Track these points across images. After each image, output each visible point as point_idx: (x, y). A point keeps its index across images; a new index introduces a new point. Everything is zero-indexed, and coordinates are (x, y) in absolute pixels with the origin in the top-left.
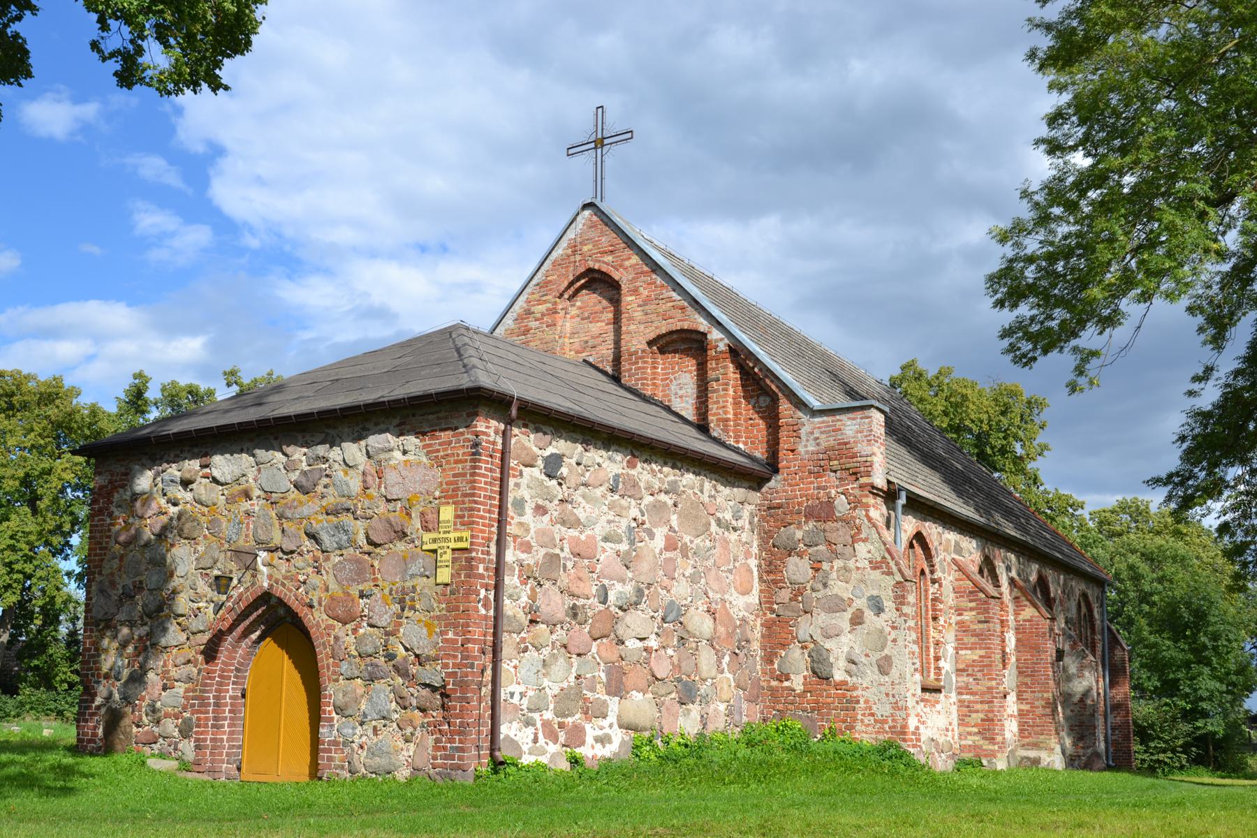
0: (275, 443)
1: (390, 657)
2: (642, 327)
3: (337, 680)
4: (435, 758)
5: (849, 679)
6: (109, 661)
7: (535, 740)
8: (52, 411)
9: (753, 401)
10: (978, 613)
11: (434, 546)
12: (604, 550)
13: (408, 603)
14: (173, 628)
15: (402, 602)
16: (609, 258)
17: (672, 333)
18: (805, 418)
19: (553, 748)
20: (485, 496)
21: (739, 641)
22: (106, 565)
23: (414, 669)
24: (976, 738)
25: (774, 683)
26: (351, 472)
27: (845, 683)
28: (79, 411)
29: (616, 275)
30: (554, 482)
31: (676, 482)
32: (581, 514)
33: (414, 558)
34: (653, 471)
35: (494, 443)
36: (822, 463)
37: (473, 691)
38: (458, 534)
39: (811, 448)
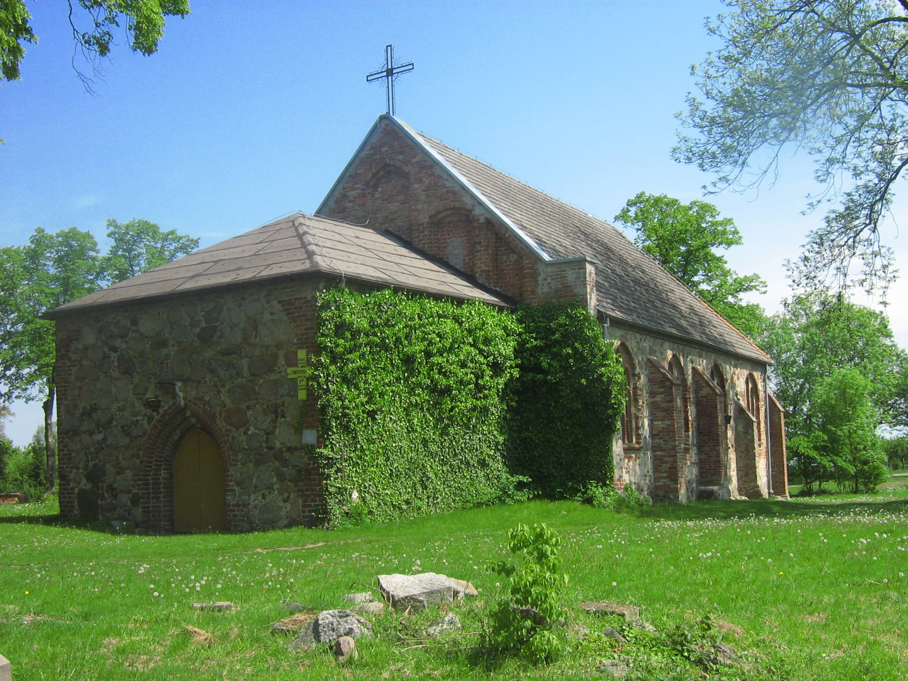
2: (426, 206)
3: (236, 465)
4: (304, 512)
10: (666, 396)
11: (295, 376)
15: (276, 412)
16: (401, 157)
24: (666, 480)
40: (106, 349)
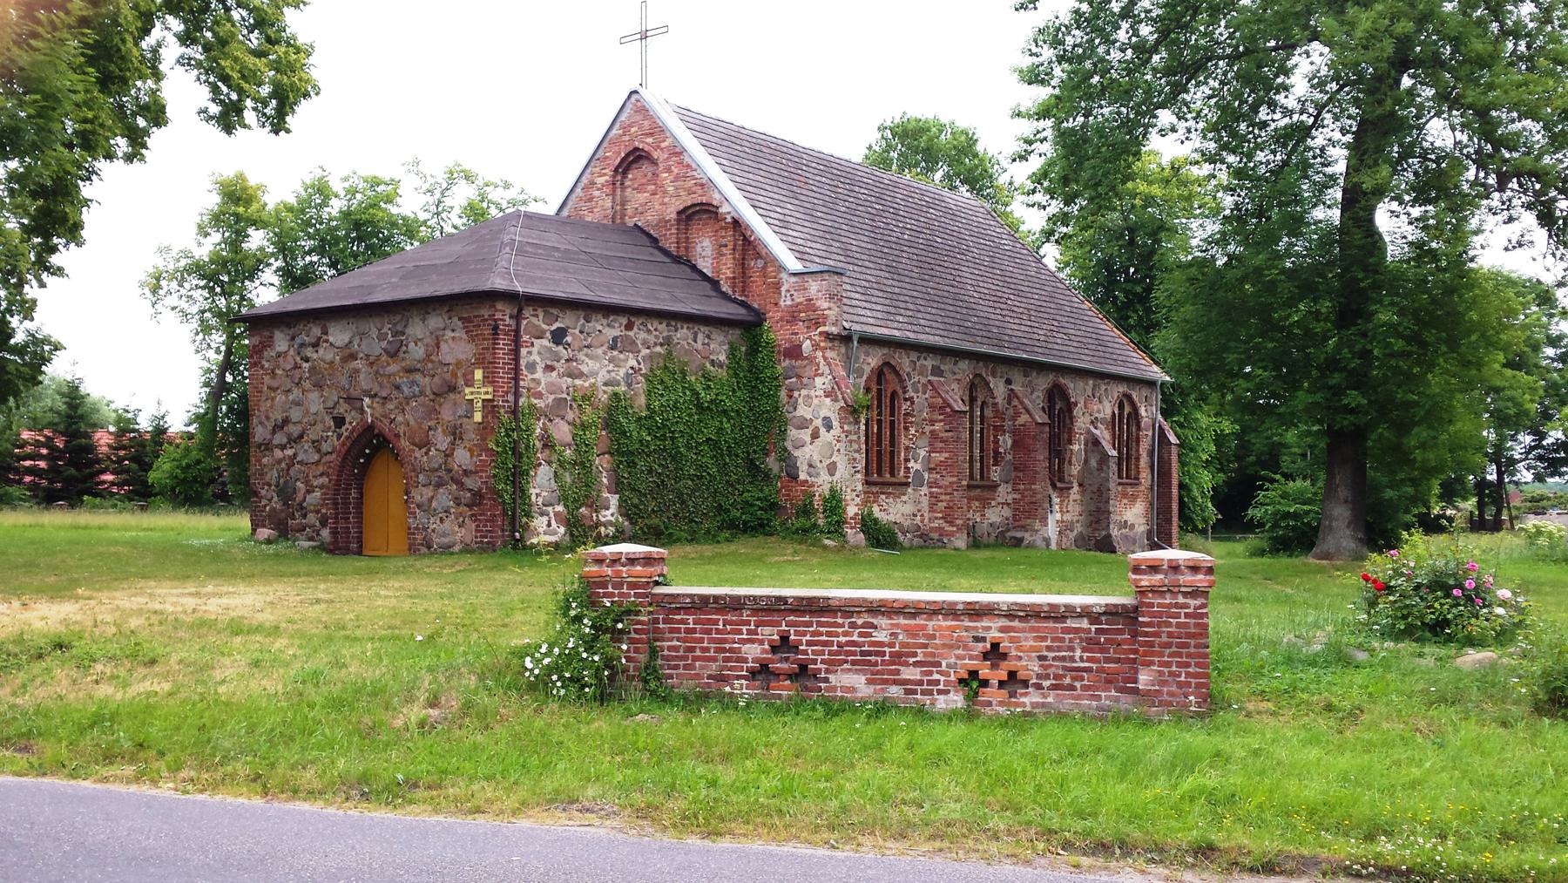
7: (549, 525)
15: (454, 434)
16: (650, 140)
17: (694, 205)
29: (655, 155)
30: (561, 348)
32: (584, 369)
40: (298, 359)
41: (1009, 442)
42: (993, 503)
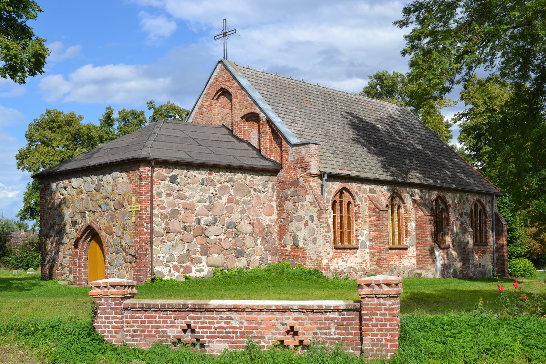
0: (88, 174)
1: (122, 246)
3: (108, 254)
4: (134, 278)
5: (304, 246)
6: (49, 247)
7: (170, 271)
8: (71, 129)
9: (276, 140)
12: (198, 206)
13: (125, 228)
14: (65, 238)
15: (124, 228)
16: (228, 84)
17: (249, 114)
18: (290, 148)
19: (177, 274)
20: (145, 193)
21: (267, 233)
22: (45, 216)
23: (128, 250)
24: (376, 266)
25: (282, 248)
26: (109, 185)
27: (302, 248)
28: (82, 128)
29: (230, 90)
30: (175, 185)
31: (232, 178)
32: (187, 194)
33: (126, 213)
34: (221, 175)
35: (147, 175)
36: (295, 165)
37: (144, 257)
38: (136, 206)
39: (292, 159)
41: (414, 226)
42: (406, 256)
